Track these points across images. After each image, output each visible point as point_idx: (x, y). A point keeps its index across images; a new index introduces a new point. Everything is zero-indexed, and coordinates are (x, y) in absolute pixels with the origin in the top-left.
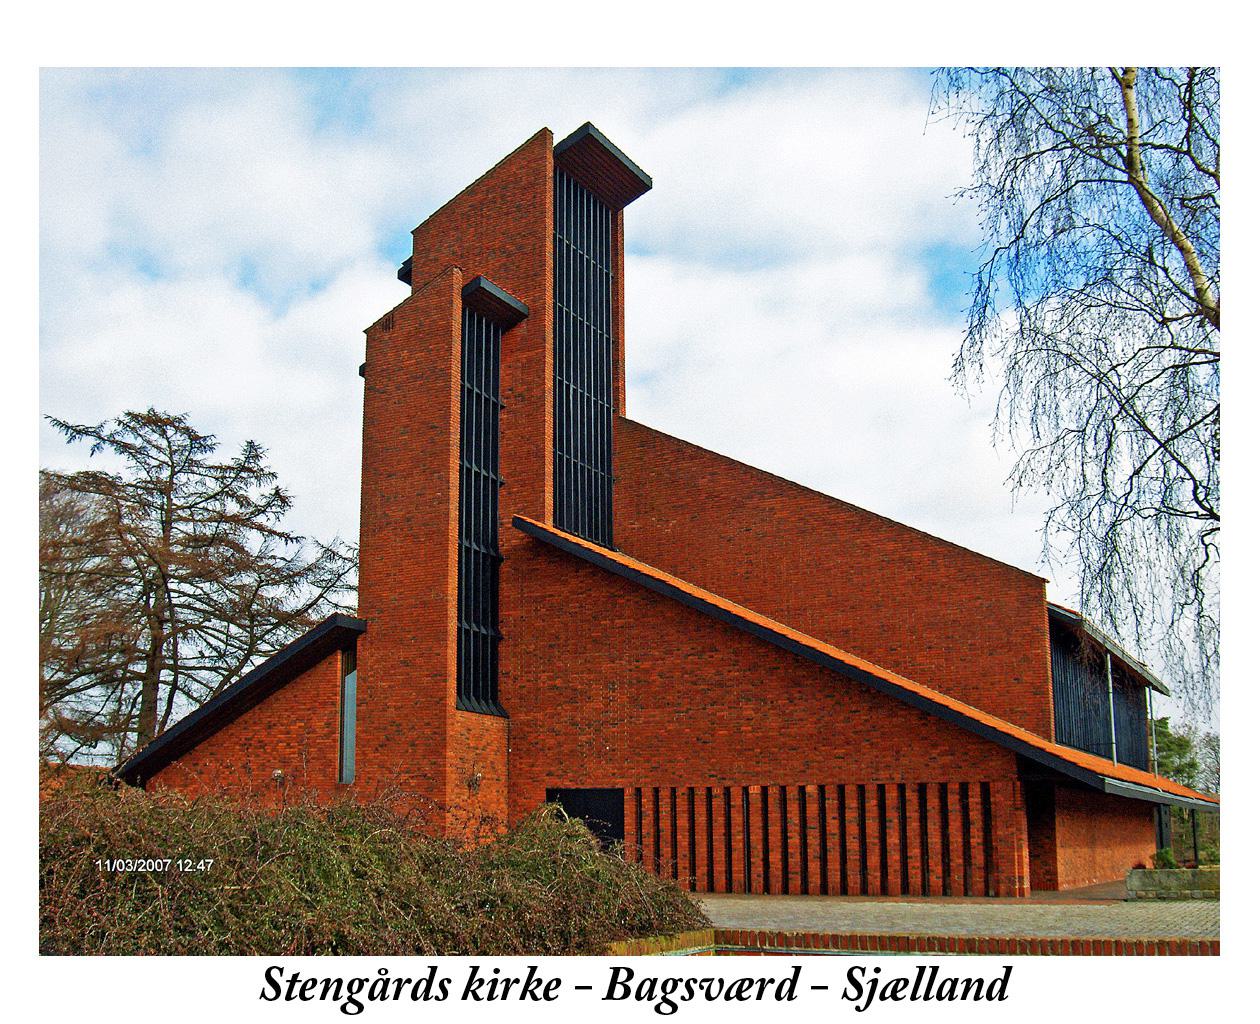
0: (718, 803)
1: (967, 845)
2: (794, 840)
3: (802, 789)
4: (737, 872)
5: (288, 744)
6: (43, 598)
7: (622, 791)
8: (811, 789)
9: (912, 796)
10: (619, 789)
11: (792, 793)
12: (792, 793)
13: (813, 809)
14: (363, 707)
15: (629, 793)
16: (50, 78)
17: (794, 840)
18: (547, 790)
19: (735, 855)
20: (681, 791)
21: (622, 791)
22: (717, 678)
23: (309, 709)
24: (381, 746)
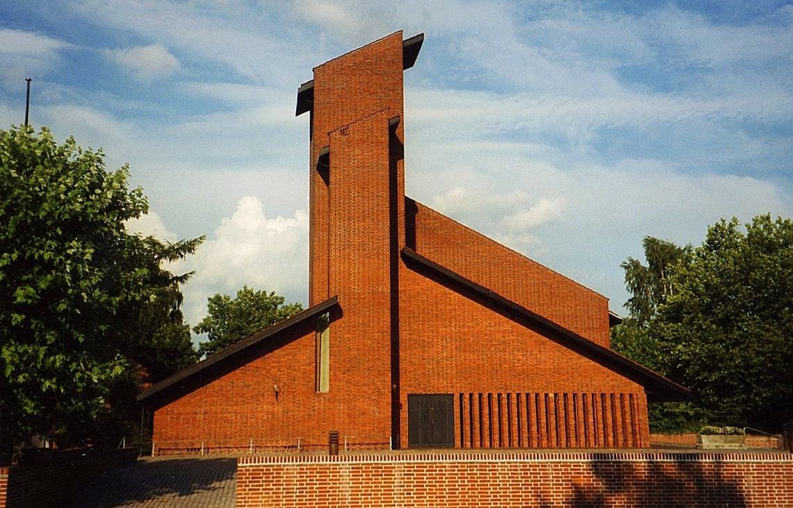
0: (505, 402)
1: (624, 422)
2: (544, 421)
3: (546, 395)
4: (516, 437)
5: (279, 370)
6: (223, 460)
7: (453, 395)
8: (551, 395)
9: (599, 399)
10: (450, 394)
11: (542, 397)
12: (542, 397)
13: (552, 405)
14: (335, 349)
15: (456, 398)
16: (145, 209)
17: (544, 421)
18: (408, 395)
19: (459, 415)
20: (485, 396)
21: (453, 395)
22: (503, 339)
23: (294, 349)
24: (347, 371)
